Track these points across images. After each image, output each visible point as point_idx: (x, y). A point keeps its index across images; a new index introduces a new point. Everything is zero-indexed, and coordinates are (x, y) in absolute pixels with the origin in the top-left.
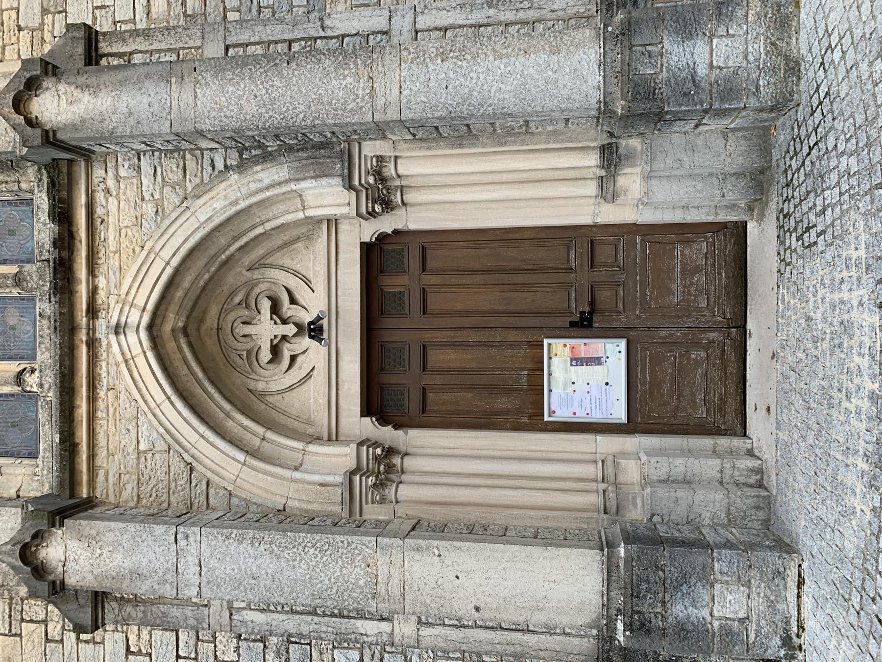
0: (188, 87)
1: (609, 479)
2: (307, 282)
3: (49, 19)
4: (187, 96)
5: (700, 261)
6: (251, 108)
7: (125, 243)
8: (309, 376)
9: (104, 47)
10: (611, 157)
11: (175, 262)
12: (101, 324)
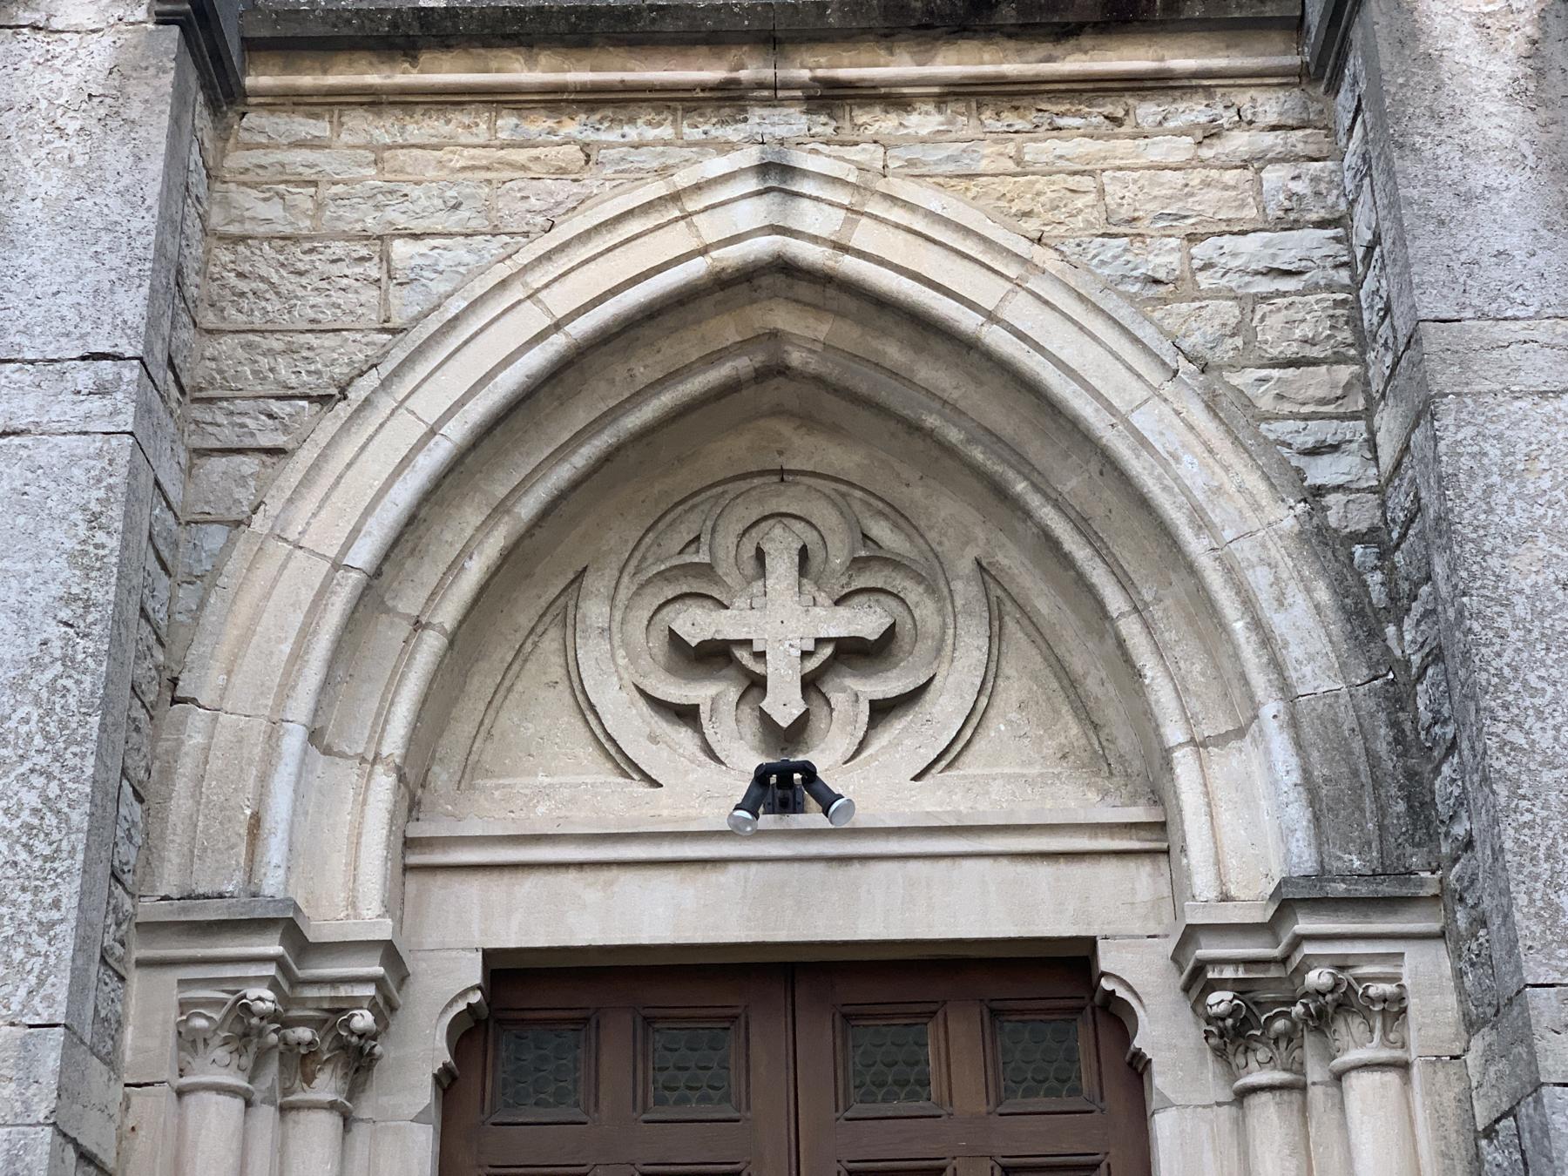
2: (948, 757)
7: (1050, 188)
8: (628, 767)
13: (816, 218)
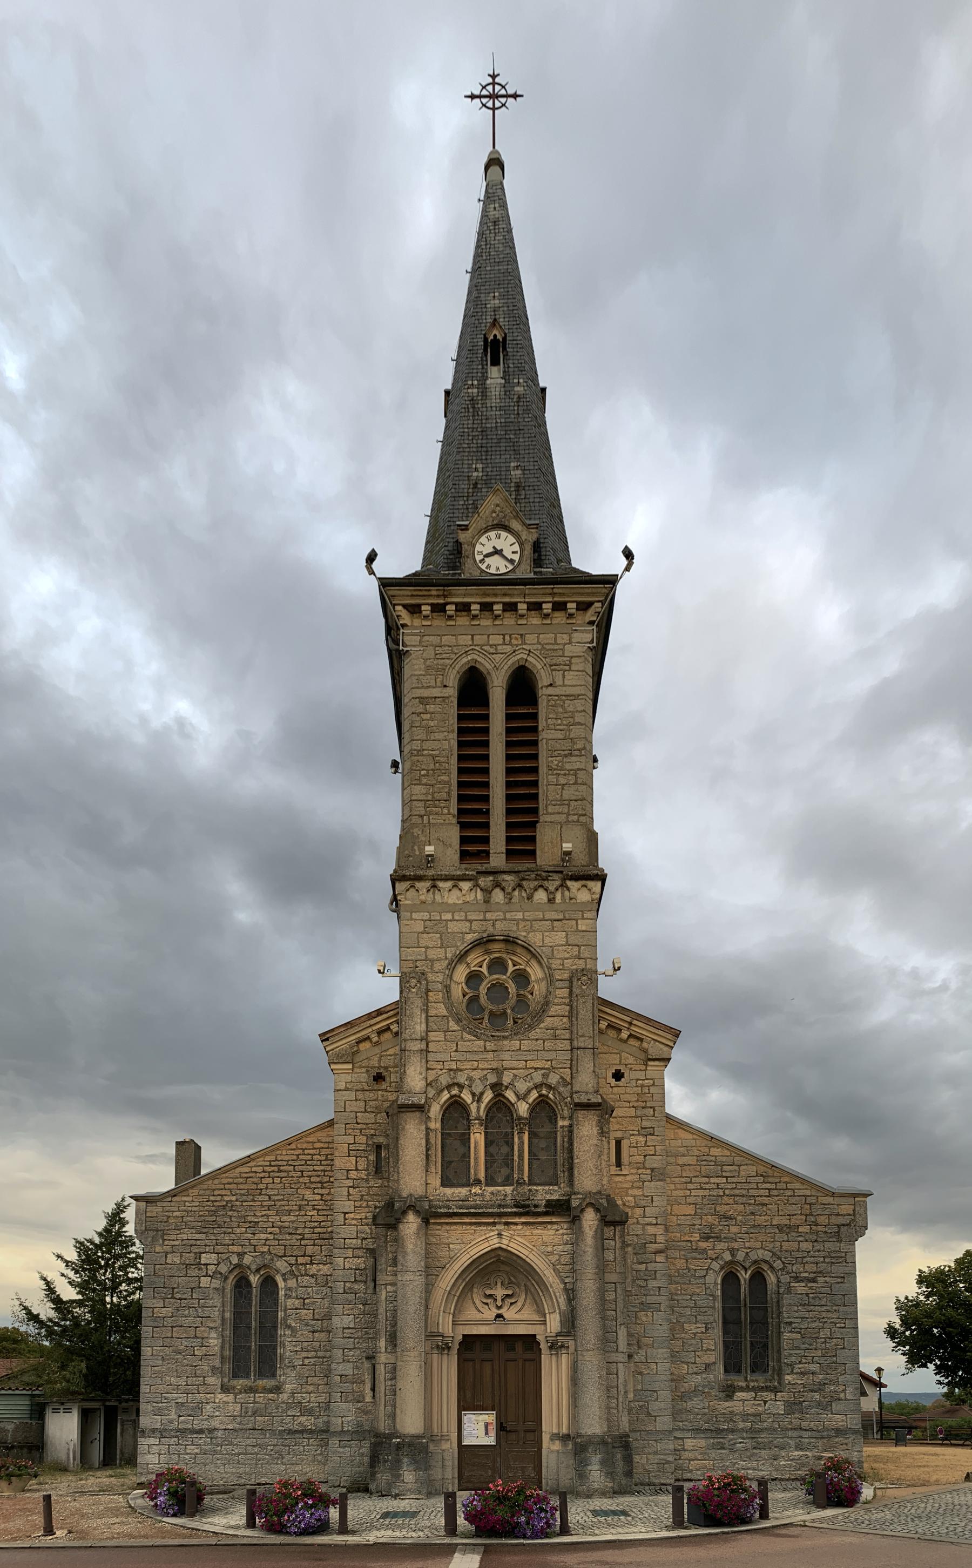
0: (594, 1277)
1: (444, 1438)
2: (520, 1311)
3: (649, 1172)
4: (590, 1276)
5: (527, 1474)
6: (584, 1303)
7: (536, 1238)
8: (479, 1311)
9: (619, 1228)
10: (565, 1438)
11: (527, 1260)
12: (502, 1227)
13: (505, 1242)
